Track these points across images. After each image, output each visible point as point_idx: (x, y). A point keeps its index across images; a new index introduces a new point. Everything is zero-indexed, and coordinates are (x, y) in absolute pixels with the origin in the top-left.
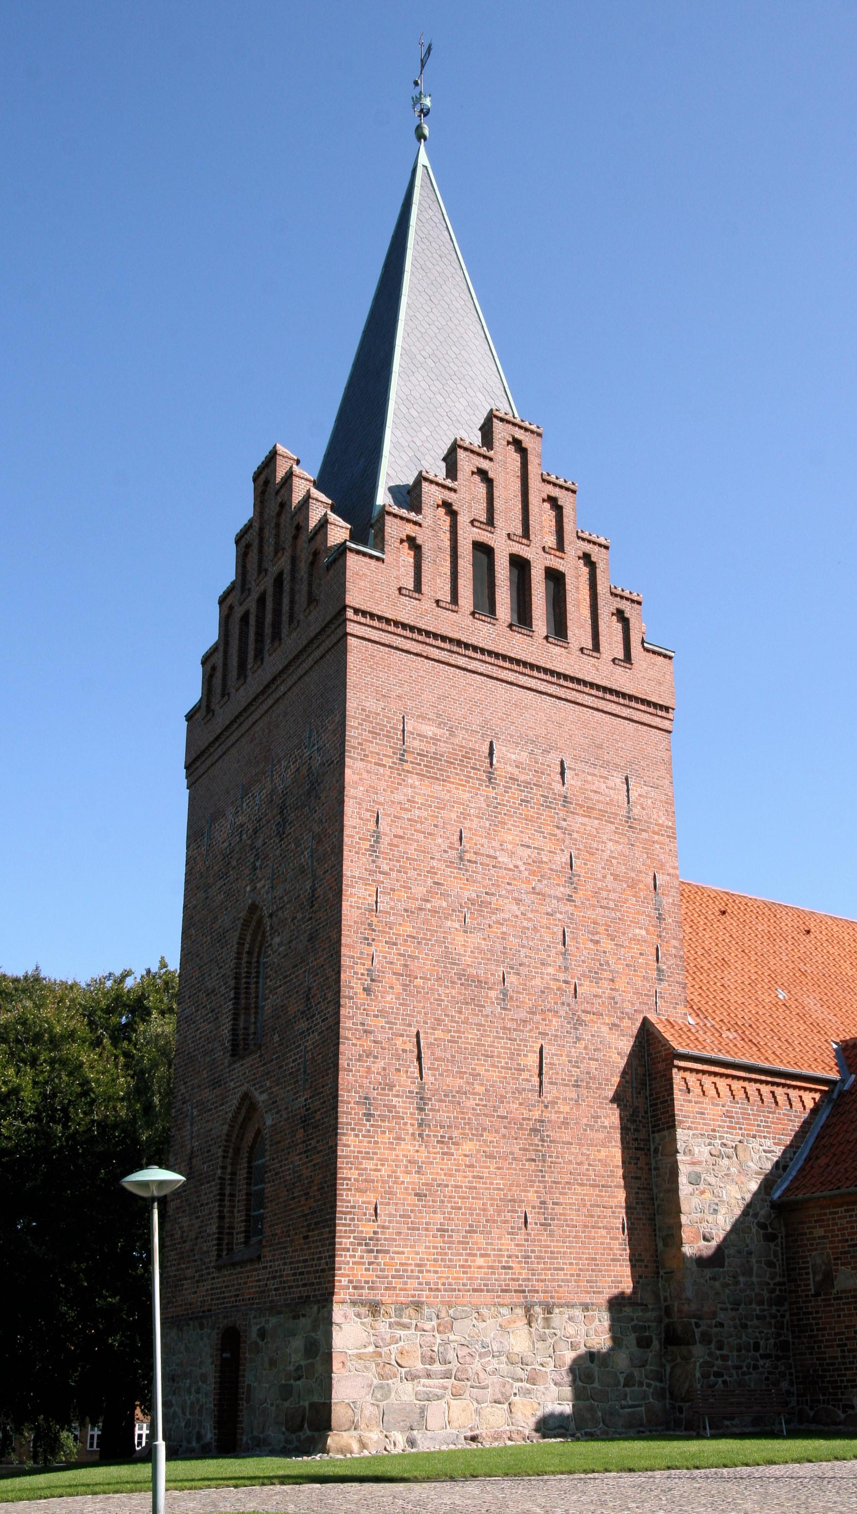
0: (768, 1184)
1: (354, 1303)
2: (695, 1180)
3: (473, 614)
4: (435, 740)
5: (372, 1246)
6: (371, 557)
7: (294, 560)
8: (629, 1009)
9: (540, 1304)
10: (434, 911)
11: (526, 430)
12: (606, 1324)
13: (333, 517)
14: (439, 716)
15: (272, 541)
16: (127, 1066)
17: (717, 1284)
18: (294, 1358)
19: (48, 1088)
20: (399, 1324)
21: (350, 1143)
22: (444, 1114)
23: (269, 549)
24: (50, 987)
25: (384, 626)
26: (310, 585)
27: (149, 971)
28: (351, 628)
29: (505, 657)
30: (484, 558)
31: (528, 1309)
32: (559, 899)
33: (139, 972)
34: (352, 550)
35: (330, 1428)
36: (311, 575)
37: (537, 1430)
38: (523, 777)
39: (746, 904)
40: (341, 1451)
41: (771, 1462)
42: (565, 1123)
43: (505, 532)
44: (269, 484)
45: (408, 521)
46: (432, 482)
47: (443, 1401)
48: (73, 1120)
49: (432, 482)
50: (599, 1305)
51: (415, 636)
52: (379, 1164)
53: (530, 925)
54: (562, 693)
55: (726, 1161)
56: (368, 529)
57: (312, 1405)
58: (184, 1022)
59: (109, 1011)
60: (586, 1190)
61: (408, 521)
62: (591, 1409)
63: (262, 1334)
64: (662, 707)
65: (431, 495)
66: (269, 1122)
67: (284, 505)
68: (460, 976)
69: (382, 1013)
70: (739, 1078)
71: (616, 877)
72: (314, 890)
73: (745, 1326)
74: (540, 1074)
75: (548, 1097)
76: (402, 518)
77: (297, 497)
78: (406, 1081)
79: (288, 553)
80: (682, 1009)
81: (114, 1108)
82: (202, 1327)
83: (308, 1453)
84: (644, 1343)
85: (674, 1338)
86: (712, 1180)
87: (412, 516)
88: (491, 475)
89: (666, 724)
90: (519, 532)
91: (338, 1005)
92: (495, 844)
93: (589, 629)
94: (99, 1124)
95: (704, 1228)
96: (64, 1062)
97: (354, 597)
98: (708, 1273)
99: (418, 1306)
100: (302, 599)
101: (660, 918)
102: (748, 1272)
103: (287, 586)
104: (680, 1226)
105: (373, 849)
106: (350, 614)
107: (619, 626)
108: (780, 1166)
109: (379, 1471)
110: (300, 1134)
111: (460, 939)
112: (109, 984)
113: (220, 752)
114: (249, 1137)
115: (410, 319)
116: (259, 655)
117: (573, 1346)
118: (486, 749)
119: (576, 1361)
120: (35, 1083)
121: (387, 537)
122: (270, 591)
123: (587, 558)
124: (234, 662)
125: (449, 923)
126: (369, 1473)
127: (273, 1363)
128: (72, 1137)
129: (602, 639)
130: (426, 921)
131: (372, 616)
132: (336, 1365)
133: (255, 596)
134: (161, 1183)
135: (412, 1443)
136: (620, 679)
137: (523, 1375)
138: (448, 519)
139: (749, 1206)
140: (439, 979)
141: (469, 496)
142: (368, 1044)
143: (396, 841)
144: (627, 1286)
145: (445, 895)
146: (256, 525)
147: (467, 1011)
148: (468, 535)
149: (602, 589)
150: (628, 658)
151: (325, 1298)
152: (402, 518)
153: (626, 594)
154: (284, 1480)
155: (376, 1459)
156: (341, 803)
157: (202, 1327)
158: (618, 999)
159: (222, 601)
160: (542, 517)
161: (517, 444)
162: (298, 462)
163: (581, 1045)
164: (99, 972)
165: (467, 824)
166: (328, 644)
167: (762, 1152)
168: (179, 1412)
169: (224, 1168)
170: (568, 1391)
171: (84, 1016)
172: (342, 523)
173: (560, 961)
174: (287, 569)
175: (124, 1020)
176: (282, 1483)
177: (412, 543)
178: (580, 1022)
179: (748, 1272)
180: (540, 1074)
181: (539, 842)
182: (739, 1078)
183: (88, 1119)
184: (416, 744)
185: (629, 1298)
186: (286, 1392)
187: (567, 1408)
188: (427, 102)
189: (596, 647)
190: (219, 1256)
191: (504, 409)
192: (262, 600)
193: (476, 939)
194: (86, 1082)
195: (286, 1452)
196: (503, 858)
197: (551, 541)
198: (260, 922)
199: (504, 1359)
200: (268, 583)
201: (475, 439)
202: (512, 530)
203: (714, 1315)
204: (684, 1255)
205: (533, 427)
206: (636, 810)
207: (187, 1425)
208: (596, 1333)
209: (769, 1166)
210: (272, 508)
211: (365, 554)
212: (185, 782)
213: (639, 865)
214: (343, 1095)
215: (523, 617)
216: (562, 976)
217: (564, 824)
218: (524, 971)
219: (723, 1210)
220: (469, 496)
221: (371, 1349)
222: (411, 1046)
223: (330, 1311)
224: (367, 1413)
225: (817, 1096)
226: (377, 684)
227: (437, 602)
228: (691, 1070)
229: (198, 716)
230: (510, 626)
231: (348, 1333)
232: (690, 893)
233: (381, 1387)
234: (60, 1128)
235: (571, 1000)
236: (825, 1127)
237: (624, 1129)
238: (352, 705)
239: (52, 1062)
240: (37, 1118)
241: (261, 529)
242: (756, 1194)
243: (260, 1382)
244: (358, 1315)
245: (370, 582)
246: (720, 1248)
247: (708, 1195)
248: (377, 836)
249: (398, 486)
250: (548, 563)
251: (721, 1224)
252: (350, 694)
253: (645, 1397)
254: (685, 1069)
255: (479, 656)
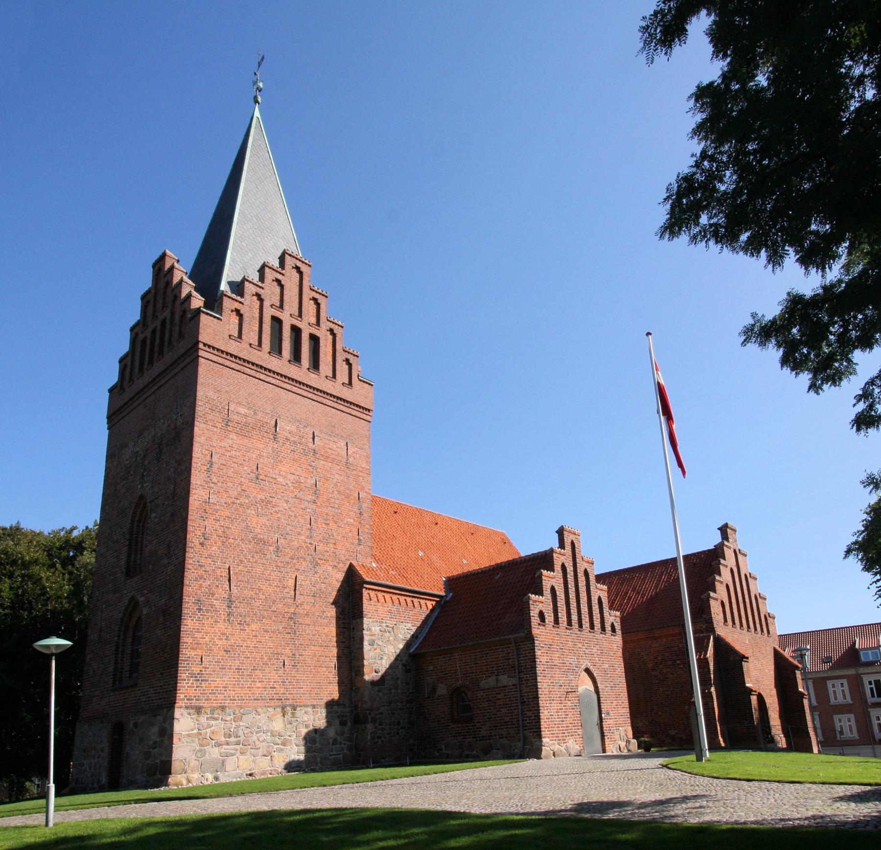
0: (408, 645)
1: (187, 708)
2: (372, 643)
3: (269, 353)
4: (246, 416)
5: (199, 678)
6: (215, 317)
7: (173, 313)
8: (343, 559)
9: (290, 705)
10: (241, 505)
11: (303, 262)
12: (324, 715)
13: (194, 293)
14: (248, 404)
15: (161, 301)
16: (70, 580)
17: (381, 694)
18: (153, 737)
19: (20, 591)
20: (212, 718)
21: (189, 624)
22: (241, 609)
23: (159, 305)
24: (25, 535)
25: (220, 354)
26: (180, 328)
27: (87, 528)
28: (201, 353)
29: (286, 377)
30: (277, 325)
31: (283, 708)
32: (309, 502)
33: (82, 527)
34: (204, 312)
35: (170, 773)
36: (181, 322)
37: (285, 769)
38: (292, 439)
39: (407, 508)
40: (177, 785)
41: (394, 778)
42: (307, 615)
43: (289, 313)
44: (161, 271)
45: (237, 301)
46: (250, 282)
47: (235, 757)
48: (34, 609)
49: (250, 282)
50: (321, 706)
51: (237, 361)
52: (205, 636)
53: (293, 514)
54: (315, 397)
55: (388, 634)
56: (214, 302)
57: (162, 762)
58: (100, 557)
59: (61, 548)
60: (316, 648)
61: (237, 301)
62: (314, 757)
63: (136, 725)
64: (366, 409)
65: (249, 289)
66: (145, 612)
67: (169, 283)
68: (254, 538)
69: (210, 556)
70: (396, 594)
71: (339, 492)
72: (175, 489)
73: (394, 714)
74: (295, 590)
75: (299, 602)
76: (233, 299)
77: (176, 280)
78: (222, 592)
79: (169, 309)
80: (369, 559)
81: (61, 603)
82: (102, 723)
83: (158, 787)
84: (343, 723)
85: (358, 720)
86: (380, 643)
87: (239, 298)
88: (283, 282)
89: (368, 418)
90: (297, 314)
91: (185, 551)
92: (277, 472)
93: (331, 367)
94: (51, 611)
95: (375, 667)
96: (30, 577)
97: (204, 337)
98: (376, 688)
99: (223, 708)
100: (176, 335)
101: (361, 514)
102: (396, 688)
103: (168, 326)
104: (363, 666)
105: (208, 470)
106: (201, 346)
107: (347, 367)
108: (414, 637)
109: (191, 794)
110: (161, 619)
111: (255, 520)
112: (62, 533)
113: (127, 411)
114: (134, 619)
115: (245, 195)
116: (151, 362)
117: (307, 726)
118: (273, 423)
119: (308, 734)
120: (11, 588)
121: (224, 308)
122: (159, 328)
123: (331, 331)
124: (137, 363)
125: (249, 511)
126: (186, 795)
127: (141, 740)
128: (34, 618)
129: (337, 372)
130: (236, 510)
131: (214, 348)
132: (175, 740)
133: (150, 329)
134: (58, 646)
135: (216, 778)
136: (346, 393)
137: (279, 742)
138: (258, 303)
139: (398, 656)
140: (242, 540)
141: (271, 293)
142: (201, 572)
143: (222, 467)
144: (336, 696)
145: (248, 497)
146: (153, 291)
147: (257, 556)
148: (268, 312)
149: (339, 347)
150: (350, 383)
151: (170, 705)
152: (233, 299)
153: (351, 351)
154: (137, 801)
155: (194, 788)
156: (192, 445)
157: (102, 723)
158: (337, 553)
159: (132, 330)
160: (309, 308)
161: (297, 268)
162: (178, 261)
163: (317, 576)
164: (56, 527)
165: (261, 460)
166: (188, 360)
167: (406, 630)
168: (88, 769)
169: (119, 636)
170: (302, 749)
171: (44, 550)
172: (200, 297)
173: (308, 533)
174: (169, 318)
175: (71, 554)
176: (136, 803)
177: (238, 312)
178: (317, 564)
179: (396, 688)
180: (295, 590)
181: (300, 472)
182: (396, 594)
183: (44, 609)
184: (235, 417)
185: (337, 701)
186: (147, 755)
187: (302, 757)
188: (261, 85)
189: (334, 376)
190: (114, 684)
191: (294, 248)
192: (154, 332)
193: (264, 520)
194: (44, 588)
195: (146, 787)
196: (280, 479)
197: (313, 320)
198: (145, 504)
199: (269, 734)
200: (158, 324)
201: (276, 264)
202: (232, 333)
203: (379, 709)
204: (364, 680)
205: (307, 262)
206: (351, 460)
207: (92, 775)
208: (318, 719)
209: (409, 636)
210: (162, 284)
211: (211, 315)
212: (106, 426)
213: (351, 487)
214: (186, 599)
215: (296, 357)
216: (309, 541)
217: (313, 464)
218: (289, 537)
219: (385, 658)
220: (271, 293)
221: (196, 731)
222: (226, 574)
223: (173, 712)
224: (192, 764)
225: (434, 603)
226: (213, 383)
227: (250, 345)
228: (372, 590)
229: (115, 391)
230: (289, 361)
231: (183, 723)
232: (376, 501)
233: (201, 751)
234: (26, 613)
235: (313, 553)
236: (437, 618)
237: (338, 618)
238: (200, 393)
239: (23, 576)
240: (12, 608)
241: (156, 294)
242: (402, 650)
243: (134, 752)
244: (189, 714)
245: (213, 330)
246: (383, 677)
247: (378, 651)
248: (211, 464)
249: (233, 282)
250: (311, 331)
251: (384, 665)
252: (199, 388)
253: (343, 750)
254: (369, 589)
255: (272, 374)
